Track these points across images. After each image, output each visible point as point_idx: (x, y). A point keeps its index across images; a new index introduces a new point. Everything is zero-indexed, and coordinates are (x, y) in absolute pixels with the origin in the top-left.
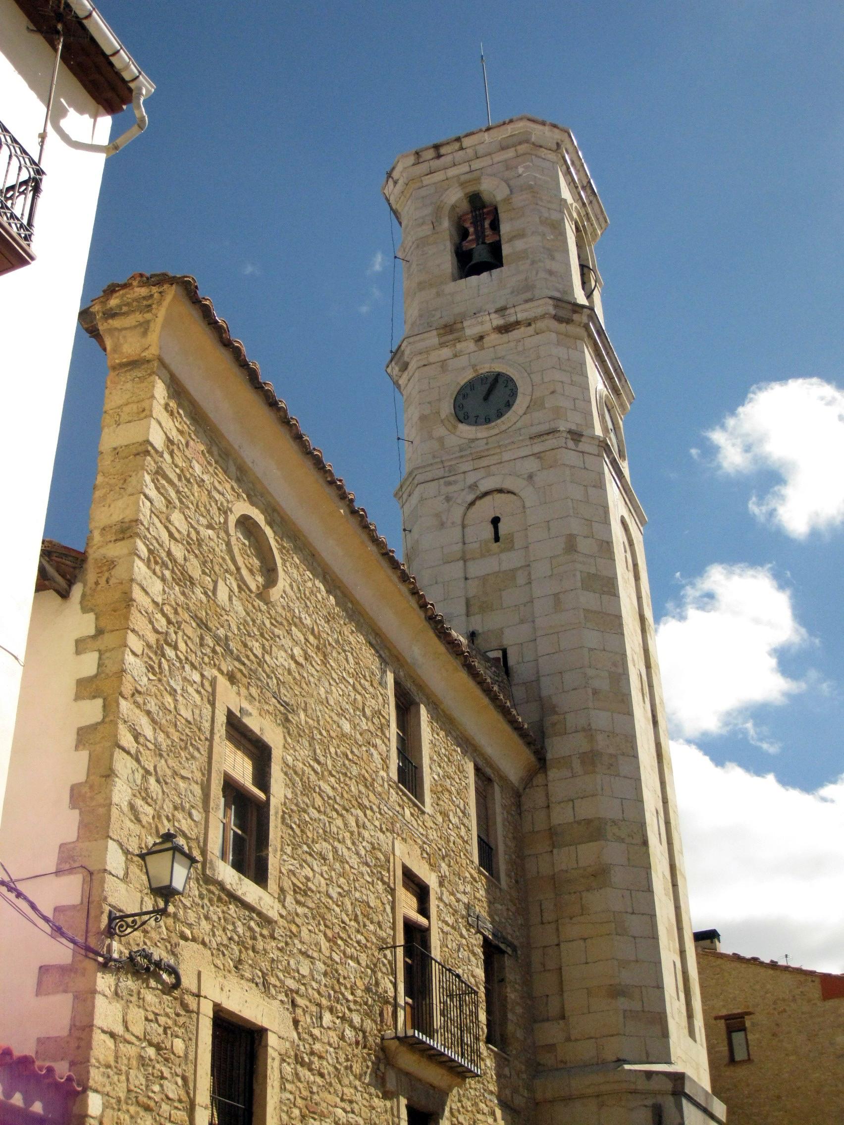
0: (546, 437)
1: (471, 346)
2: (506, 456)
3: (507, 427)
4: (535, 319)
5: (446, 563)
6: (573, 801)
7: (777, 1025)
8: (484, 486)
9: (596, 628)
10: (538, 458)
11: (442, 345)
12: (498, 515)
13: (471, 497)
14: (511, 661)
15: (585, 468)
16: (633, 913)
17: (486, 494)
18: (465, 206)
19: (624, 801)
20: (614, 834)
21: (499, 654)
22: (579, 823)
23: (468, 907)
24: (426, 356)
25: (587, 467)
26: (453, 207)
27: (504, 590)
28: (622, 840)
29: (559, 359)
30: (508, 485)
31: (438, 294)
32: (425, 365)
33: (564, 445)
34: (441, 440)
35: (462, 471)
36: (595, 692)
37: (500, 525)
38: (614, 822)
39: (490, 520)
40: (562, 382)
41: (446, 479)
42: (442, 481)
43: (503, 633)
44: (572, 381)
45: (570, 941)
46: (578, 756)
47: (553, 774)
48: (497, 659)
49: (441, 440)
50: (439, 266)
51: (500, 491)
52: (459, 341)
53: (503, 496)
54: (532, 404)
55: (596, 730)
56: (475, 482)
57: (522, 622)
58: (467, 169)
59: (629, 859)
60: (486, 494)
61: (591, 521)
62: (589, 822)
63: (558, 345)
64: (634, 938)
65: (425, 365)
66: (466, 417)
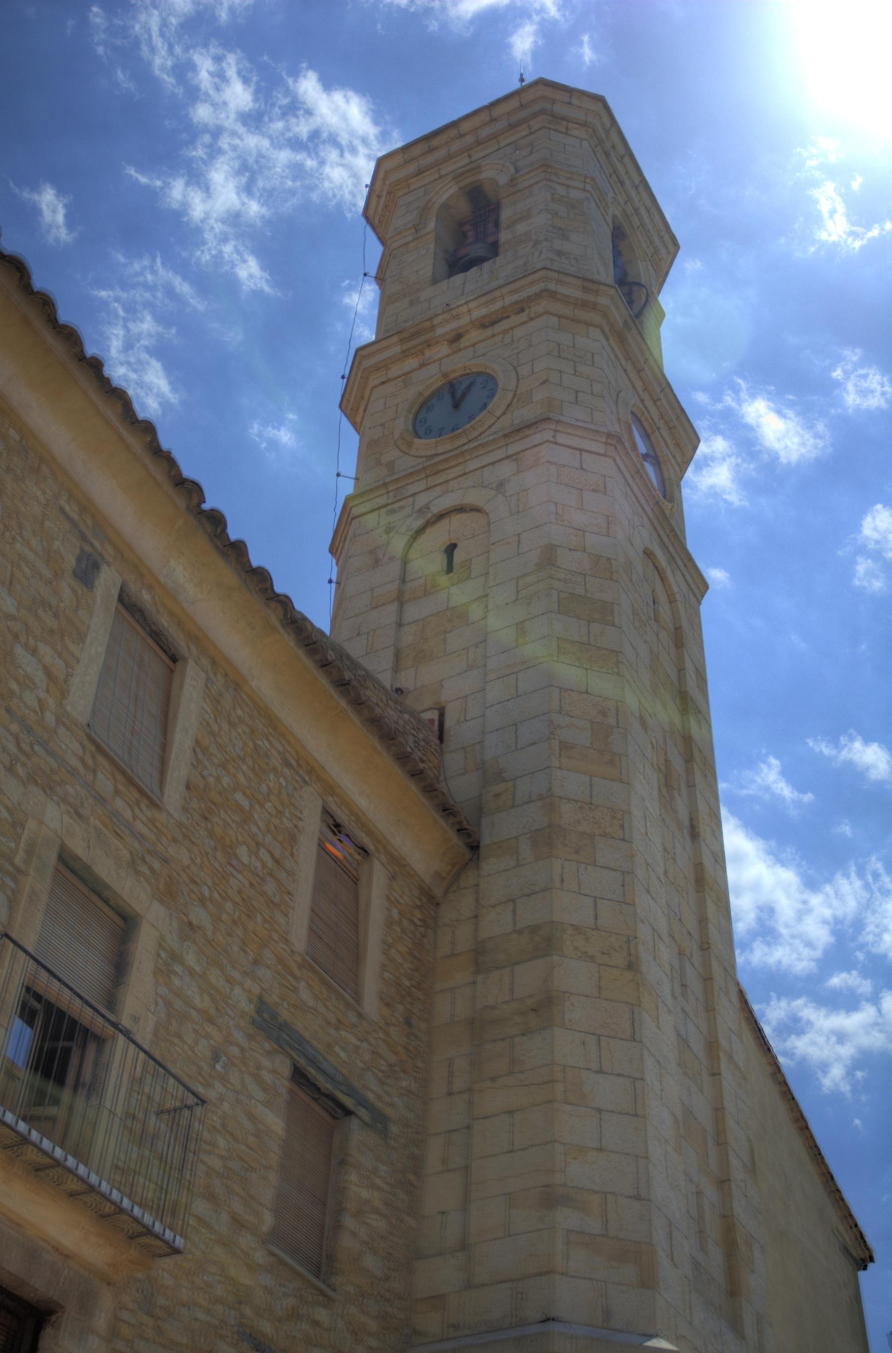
0: (527, 432)
1: (444, 349)
2: (472, 465)
3: (477, 433)
4: (530, 299)
5: (375, 608)
6: (513, 901)
7: (658, 984)
8: (437, 508)
9: (577, 663)
10: (514, 460)
11: (406, 354)
12: (453, 541)
13: (418, 523)
14: (448, 723)
15: (582, 468)
16: (600, 1071)
17: (441, 516)
18: (464, 208)
19: (599, 902)
20: (577, 948)
21: (435, 715)
22: (520, 932)
23: (63, 562)
24: (384, 372)
25: (584, 466)
26: (445, 207)
27: (449, 632)
28: (592, 958)
29: (559, 344)
30: (472, 498)
31: (412, 303)
32: (383, 383)
33: (552, 439)
34: (391, 465)
35: (410, 493)
36: (565, 746)
37: (456, 553)
38: (577, 929)
39: (443, 549)
40: (560, 372)
41: (389, 507)
42: (383, 511)
43: (442, 686)
44: (575, 371)
45: (486, 1118)
46: (528, 836)
47: (489, 865)
48: (431, 721)
49: (391, 465)
50: (417, 272)
51: (460, 509)
52: (429, 346)
53: (463, 516)
54: (516, 400)
55: (561, 798)
56: (427, 504)
57: (470, 668)
58: (467, 161)
59: (600, 988)
60: (441, 516)
61: (584, 531)
62: (534, 929)
63: (559, 330)
64: (600, 1111)
65: (383, 383)
66: (428, 432)
